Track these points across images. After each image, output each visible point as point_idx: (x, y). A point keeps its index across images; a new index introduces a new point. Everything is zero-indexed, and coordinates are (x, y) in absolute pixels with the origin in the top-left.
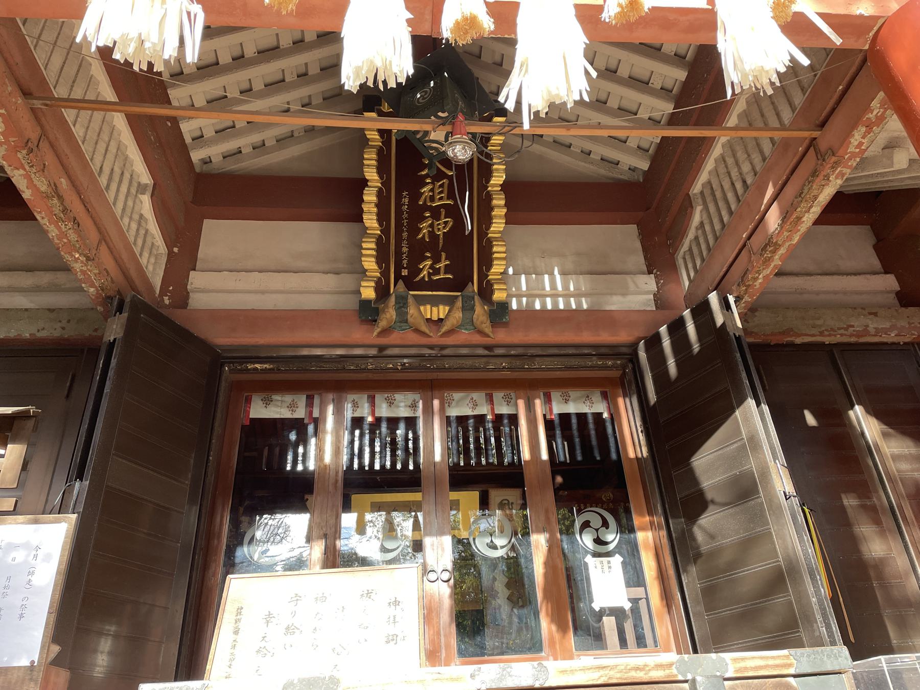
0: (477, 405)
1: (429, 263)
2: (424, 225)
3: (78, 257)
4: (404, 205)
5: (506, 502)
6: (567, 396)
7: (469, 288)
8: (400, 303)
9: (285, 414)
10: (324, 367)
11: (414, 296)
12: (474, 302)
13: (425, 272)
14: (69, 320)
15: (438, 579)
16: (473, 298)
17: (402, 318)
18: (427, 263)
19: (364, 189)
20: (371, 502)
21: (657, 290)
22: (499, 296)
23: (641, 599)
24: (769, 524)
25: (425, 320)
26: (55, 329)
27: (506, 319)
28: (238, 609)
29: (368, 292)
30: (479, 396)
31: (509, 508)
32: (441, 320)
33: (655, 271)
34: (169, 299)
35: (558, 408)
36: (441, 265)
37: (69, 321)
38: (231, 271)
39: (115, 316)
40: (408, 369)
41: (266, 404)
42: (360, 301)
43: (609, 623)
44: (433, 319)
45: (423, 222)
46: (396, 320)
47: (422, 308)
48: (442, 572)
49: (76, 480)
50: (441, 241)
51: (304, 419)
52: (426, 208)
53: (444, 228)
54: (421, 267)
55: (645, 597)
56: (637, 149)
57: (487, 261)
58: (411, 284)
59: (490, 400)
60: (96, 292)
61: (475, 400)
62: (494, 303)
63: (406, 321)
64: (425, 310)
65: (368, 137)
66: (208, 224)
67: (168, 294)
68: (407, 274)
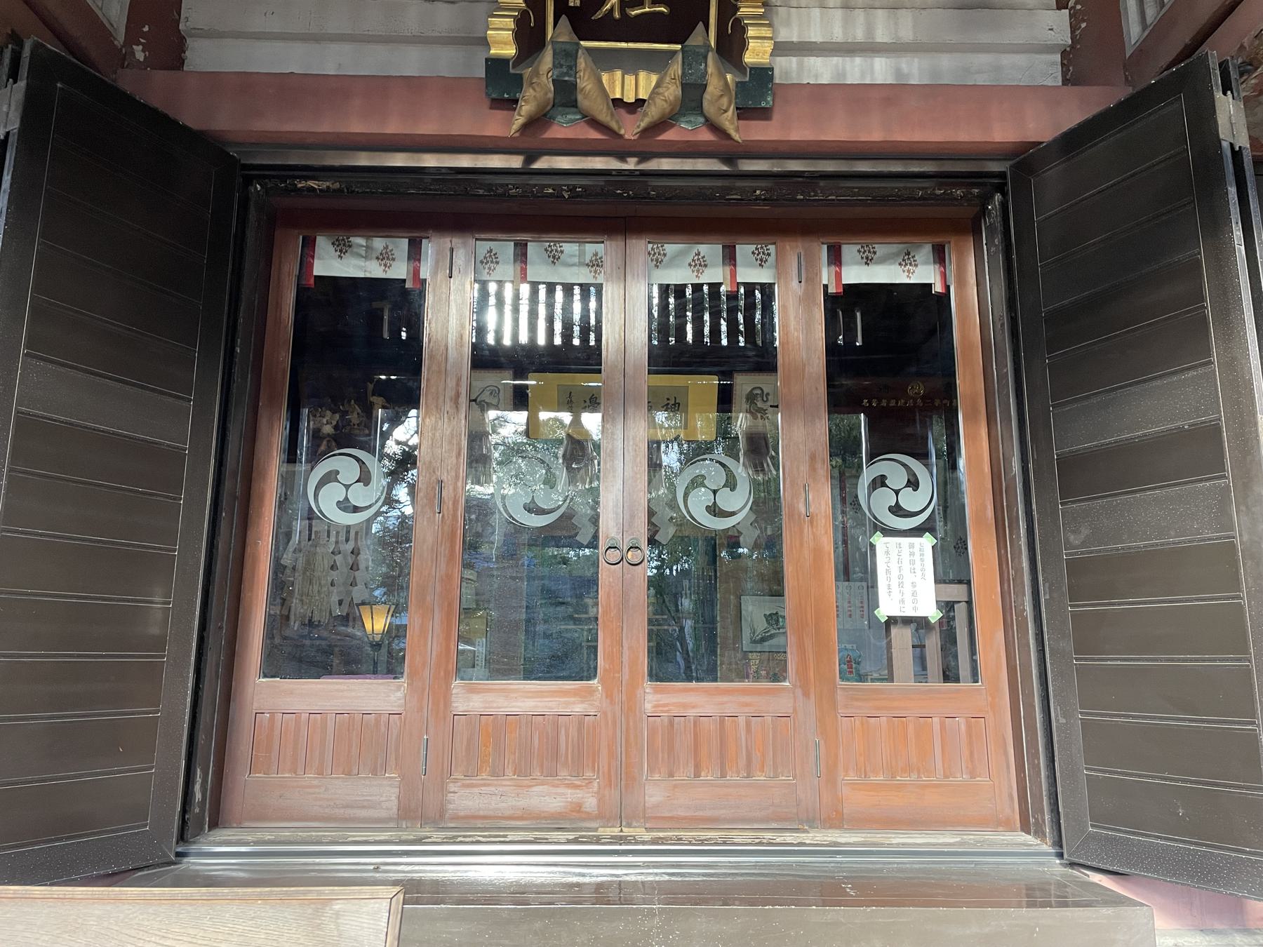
5: (759, 392)
7: (695, 39)
8: (561, 66)
9: (374, 270)
10: (431, 190)
11: (588, 50)
15: (622, 558)
16: (705, 58)
17: (566, 94)
20: (558, 385)
21: (1070, 42)
22: (757, 52)
24: (1232, 529)
30: (711, 250)
31: (763, 399)
32: (640, 102)
35: (855, 274)
39: (6, 86)
41: (341, 251)
42: (487, 60)
43: (902, 638)
44: (625, 100)
46: (556, 101)
47: (605, 77)
48: (629, 550)
51: (404, 281)
55: (966, 600)
59: (730, 257)
61: (703, 257)
62: (745, 69)
63: (574, 104)
64: (612, 82)
67: (142, 41)
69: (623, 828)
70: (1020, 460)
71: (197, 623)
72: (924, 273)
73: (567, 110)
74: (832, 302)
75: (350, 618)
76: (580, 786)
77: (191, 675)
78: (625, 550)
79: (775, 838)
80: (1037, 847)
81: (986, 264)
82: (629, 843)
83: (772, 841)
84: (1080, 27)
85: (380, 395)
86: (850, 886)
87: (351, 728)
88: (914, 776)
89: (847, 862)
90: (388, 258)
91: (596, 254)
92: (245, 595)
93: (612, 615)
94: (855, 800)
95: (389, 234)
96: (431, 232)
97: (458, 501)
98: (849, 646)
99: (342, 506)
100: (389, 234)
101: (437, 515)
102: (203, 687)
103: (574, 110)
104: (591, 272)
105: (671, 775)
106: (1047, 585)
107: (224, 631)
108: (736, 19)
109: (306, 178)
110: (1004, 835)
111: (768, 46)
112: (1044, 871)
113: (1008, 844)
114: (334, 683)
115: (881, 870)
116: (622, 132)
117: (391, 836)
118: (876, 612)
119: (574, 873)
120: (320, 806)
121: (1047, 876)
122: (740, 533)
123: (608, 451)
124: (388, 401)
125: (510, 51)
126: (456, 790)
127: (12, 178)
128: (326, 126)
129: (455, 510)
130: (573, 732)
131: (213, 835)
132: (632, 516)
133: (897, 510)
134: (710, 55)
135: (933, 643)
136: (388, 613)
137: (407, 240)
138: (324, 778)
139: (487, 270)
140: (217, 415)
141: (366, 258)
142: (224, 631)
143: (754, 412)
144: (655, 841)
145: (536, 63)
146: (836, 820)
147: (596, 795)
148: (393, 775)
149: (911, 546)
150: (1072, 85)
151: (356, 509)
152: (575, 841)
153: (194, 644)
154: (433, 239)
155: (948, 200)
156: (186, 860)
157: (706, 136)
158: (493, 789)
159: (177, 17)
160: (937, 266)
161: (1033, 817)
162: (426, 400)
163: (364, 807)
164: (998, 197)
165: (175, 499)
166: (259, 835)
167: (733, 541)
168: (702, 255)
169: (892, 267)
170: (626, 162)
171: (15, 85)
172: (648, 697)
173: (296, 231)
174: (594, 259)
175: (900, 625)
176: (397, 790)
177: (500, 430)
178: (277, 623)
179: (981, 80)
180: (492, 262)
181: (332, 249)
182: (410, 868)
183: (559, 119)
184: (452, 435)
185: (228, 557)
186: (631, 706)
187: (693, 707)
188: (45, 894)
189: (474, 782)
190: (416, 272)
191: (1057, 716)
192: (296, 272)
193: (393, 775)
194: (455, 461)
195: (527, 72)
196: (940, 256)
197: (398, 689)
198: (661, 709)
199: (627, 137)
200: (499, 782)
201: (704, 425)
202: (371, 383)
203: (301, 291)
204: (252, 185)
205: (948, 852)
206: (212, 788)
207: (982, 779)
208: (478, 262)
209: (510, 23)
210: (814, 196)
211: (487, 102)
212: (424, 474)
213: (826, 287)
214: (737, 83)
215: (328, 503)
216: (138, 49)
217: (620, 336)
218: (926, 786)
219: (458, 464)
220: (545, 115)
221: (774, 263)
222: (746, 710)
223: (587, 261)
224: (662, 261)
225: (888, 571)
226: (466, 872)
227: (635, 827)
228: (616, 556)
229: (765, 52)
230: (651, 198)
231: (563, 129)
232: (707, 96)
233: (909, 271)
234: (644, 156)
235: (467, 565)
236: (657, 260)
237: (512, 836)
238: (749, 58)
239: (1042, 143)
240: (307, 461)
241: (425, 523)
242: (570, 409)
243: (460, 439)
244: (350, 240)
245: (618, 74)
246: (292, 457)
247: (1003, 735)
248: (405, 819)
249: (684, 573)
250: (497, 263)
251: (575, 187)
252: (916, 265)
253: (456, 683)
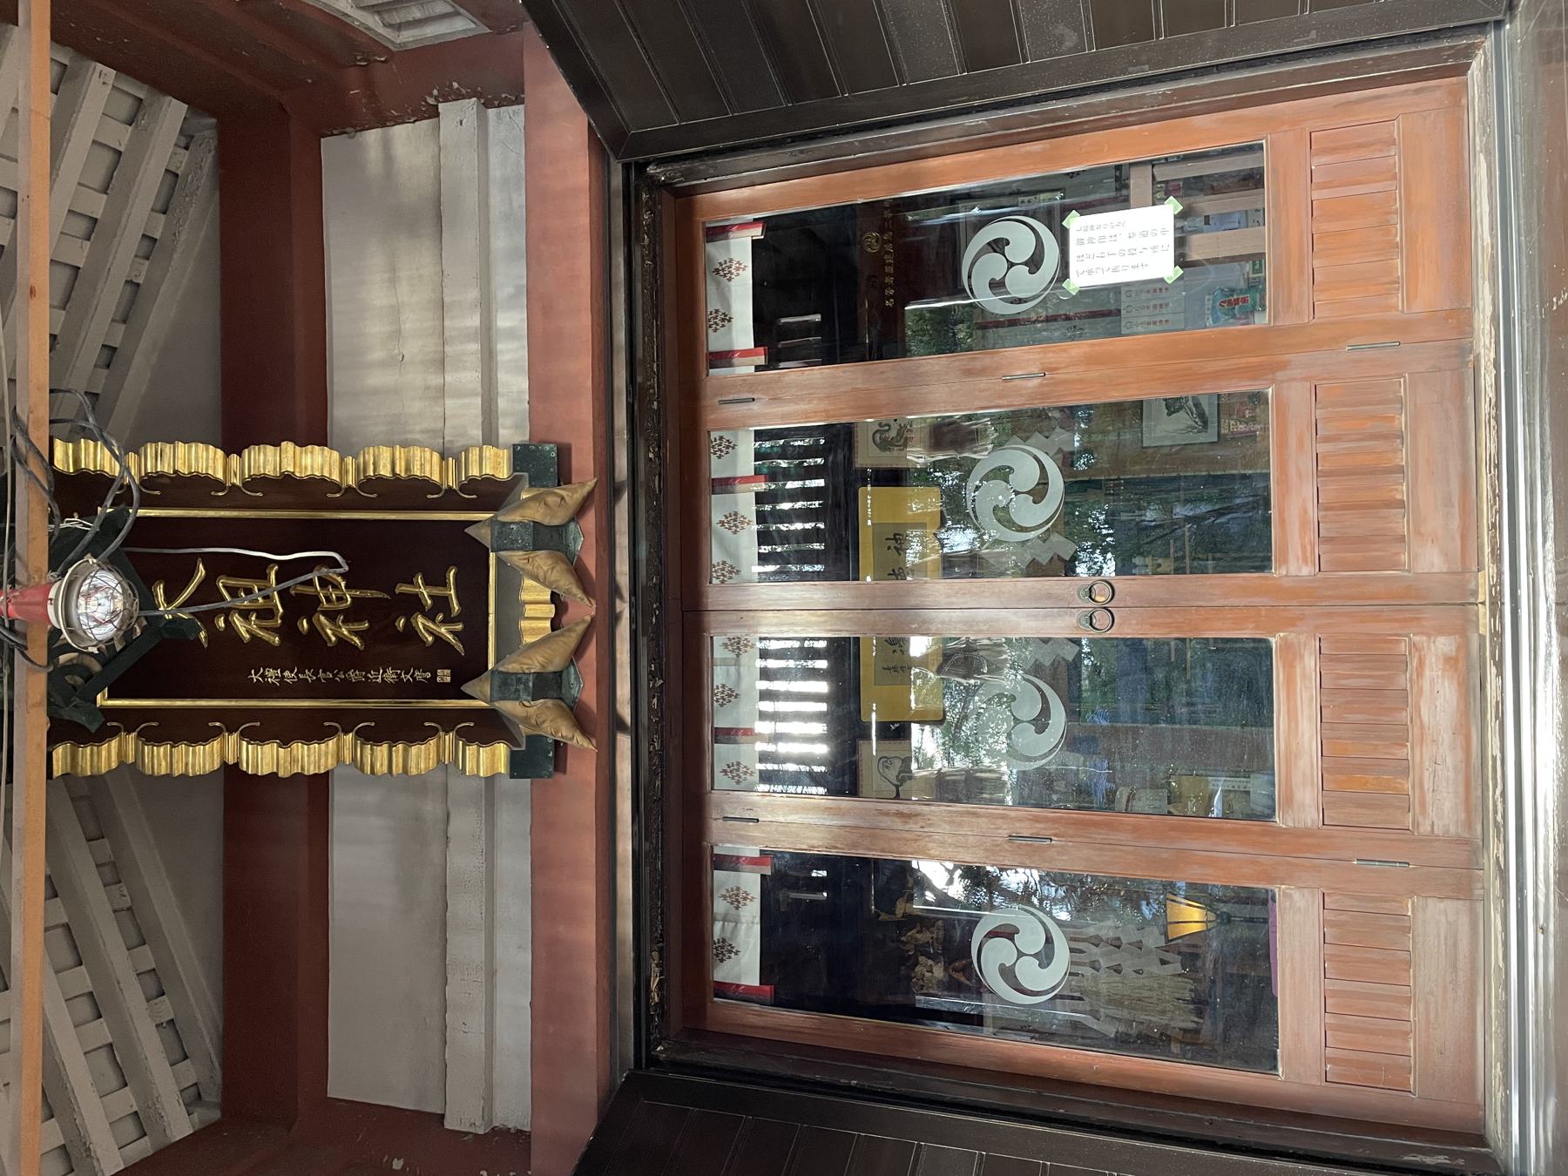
0: (736, 514)
1: (420, 622)
2: (329, 632)
4: (283, 677)
5: (878, 436)
6: (716, 318)
7: (484, 535)
8: (517, 690)
11: (498, 660)
12: (514, 523)
13: (443, 630)
15: (1105, 608)
16: (504, 524)
17: (548, 685)
18: (421, 627)
19: (245, 773)
22: (495, 464)
23: (1154, 177)
25: (557, 632)
27: (551, 450)
29: (493, 758)
30: (717, 508)
31: (887, 431)
32: (555, 598)
33: (431, 101)
35: (741, 333)
36: (425, 592)
38: (446, 1042)
40: (660, 665)
41: (730, 952)
42: (512, 777)
45: (324, 637)
48: (1093, 600)
50: (368, 594)
51: (763, 876)
52: (288, 629)
53: (336, 587)
54: (430, 639)
56: (136, 127)
57: (412, 491)
58: (470, 665)
59: (725, 485)
63: (558, 675)
64: (533, 631)
65: (114, 765)
66: (339, 1087)
68: (448, 679)
69: (1479, 600)
70: (969, 116)
71: (1206, 1153)
72: (739, 250)
73: (564, 683)
74: (774, 361)
75: (1189, 952)
76: (1420, 658)
77: (1277, 1163)
78: (1092, 604)
79: (1488, 399)
80: (1489, 55)
81: (729, 177)
82: (1501, 593)
83: (1493, 403)
84: (457, 89)
85: (894, 905)
86: (1555, 300)
88: (1395, 219)
89: (1521, 302)
90: (737, 895)
91: (725, 645)
92: (1166, 1089)
93: (1181, 620)
94: (1429, 295)
95: (709, 893)
97: (1035, 816)
98: (1208, 304)
99: (1045, 962)
100: (709, 893)
101: (1053, 842)
102: (1292, 1148)
103: (564, 674)
104: (746, 651)
105: (1402, 539)
106: (1130, 69)
107: (1216, 1118)
108: (461, 489)
110: (1474, 98)
111: (489, 451)
112: (1521, 43)
113: (1486, 93)
115: (1529, 257)
116: (588, 618)
117: (1495, 909)
118: (1169, 282)
119: (1546, 667)
120: (1454, 1002)
121: (1530, 38)
122: (1060, 450)
123: (965, 628)
124: (902, 895)
125: (502, 749)
126: (1428, 823)
128: (589, 970)
129: (1046, 820)
130: (1343, 669)
131: (1496, 1142)
132: (1049, 596)
133: (1034, 263)
134: (501, 519)
135: (1207, 204)
137: (715, 872)
138: (1415, 997)
139: (748, 776)
140: (937, 1114)
141: (737, 922)
142: (1216, 1118)
143: (902, 439)
144: (1497, 558)
145: (515, 720)
146: (1460, 318)
147: (1432, 638)
148: (1410, 906)
149: (1080, 242)
150: (523, 93)
151: (1049, 940)
152: (1500, 665)
153: (1235, 1157)
154: (713, 841)
155: (654, 229)
157: (590, 520)
158: (1426, 774)
159: (471, 1136)
160: (731, 235)
161: (1446, 61)
162: (907, 853)
163: (1455, 945)
164: (651, 170)
166: (1496, 1082)
167: (1067, 461)
168: (723, 519)
169: (733, 289)
170: (621, 613)
172: (1293, 570)
173: (709, 1004)
174: (730, 648)
175: (1187, 250)
176: (1430, 900)
177: (929, 755)
178: (1193, 1046)
179: (520, 200)
180: (738, 770)
182: (1541, 886)
183: (575, 692)
184: (950, 822)
185: (1118, 1108)
186: (1306, 594)
187: (1305, 512)
189: (1417, 800)
190: (753, 861)
191: (1308, 42)
192: (757, 1007)
193: (1410, 906)
194: (984, 819)
195: (524, 730)
196: (719, 233)
197: (1287, 896)
198: (1308, 554)
199: (593, 613)
200: (1417, 768)
201: (921, 503)
203: (778, 1003)
205: (1500, 171)
206: (1429, 1141)
207: (1396, 129)
208: (737, 787)
209: (471, 750)
210: (653, 388)
211: (559, 777)
212: (1001, 858)
213: (758, 368)
214: (531, 486)
215: (1044, 979)
217: (823, 615)
218: (1408, 201)
219: (991, 816)
220: (571, 709)
221: (730, 432)
222: (1307, 443)
223: (733, 655)
224: (731, 566)
225: (1115, 270)
226: (1546, 812)
227: (1477, 585)
228: (1103, 616)
229: (496, 455)
230: (661, 583)
231: (586, 690)
232: (547, 521)
233: (738, 269)
234: (615, 591)
235: (1110, 803)
236: (731, 572)
237: (1493, 748)
238: (503, 473)
239: (589, 124)
240: (979, 997)
241: (1065, 858)
242: (910, 669)
243: (955, 812)
245: (524, 624)
246: (976, 1020)
247: (1335, 107)
248: (1471, 890)
249: (1109, 522)
250: (738, 764)
251: (650, 673)
252: (731, 260)
253: (1278, 820)
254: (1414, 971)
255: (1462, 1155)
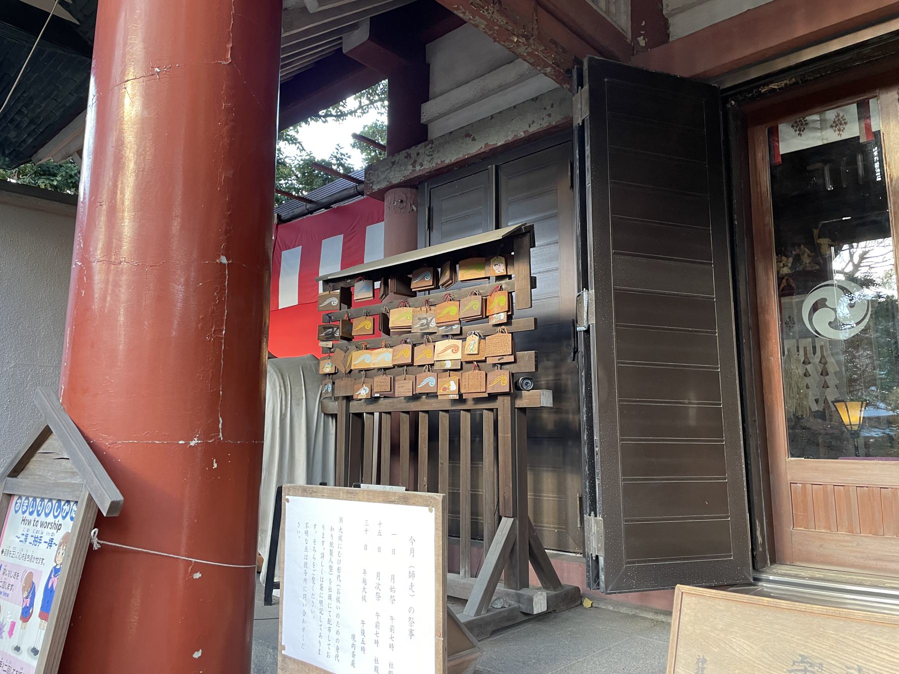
3: (517, 40)
9: (831, 136)
14: (553, 104)
26: (543, 119)
28: (698, 663)
34: (644, 39)
37: (552, 106)
39: (578, 92)
41: (800, 130)
49: (583, 290)
51: (858, 138)
60: (553, 70)
87: (872, 498)
90: (841, 124)
96: (878, 91)
102: (750, 462)
109: (767, 84)
114: (850, 463)
124: (833, 241)
127: (591, 147)
136: (861, 407)
138: (855, 535)
141: (821, 129)
156: (760, 584)
163: (893, 561)
165: (712, 333)
171: (583, 89)
181: (792, 130)
188: (791, 607)
190: (868, 128)
202: (816, 229)
203: (773, 168)
204: (728, 103)
206: (767, 534)
216: (640, 39)
244: (805, 119)
254: (871, 537)
255: (764, 550)
